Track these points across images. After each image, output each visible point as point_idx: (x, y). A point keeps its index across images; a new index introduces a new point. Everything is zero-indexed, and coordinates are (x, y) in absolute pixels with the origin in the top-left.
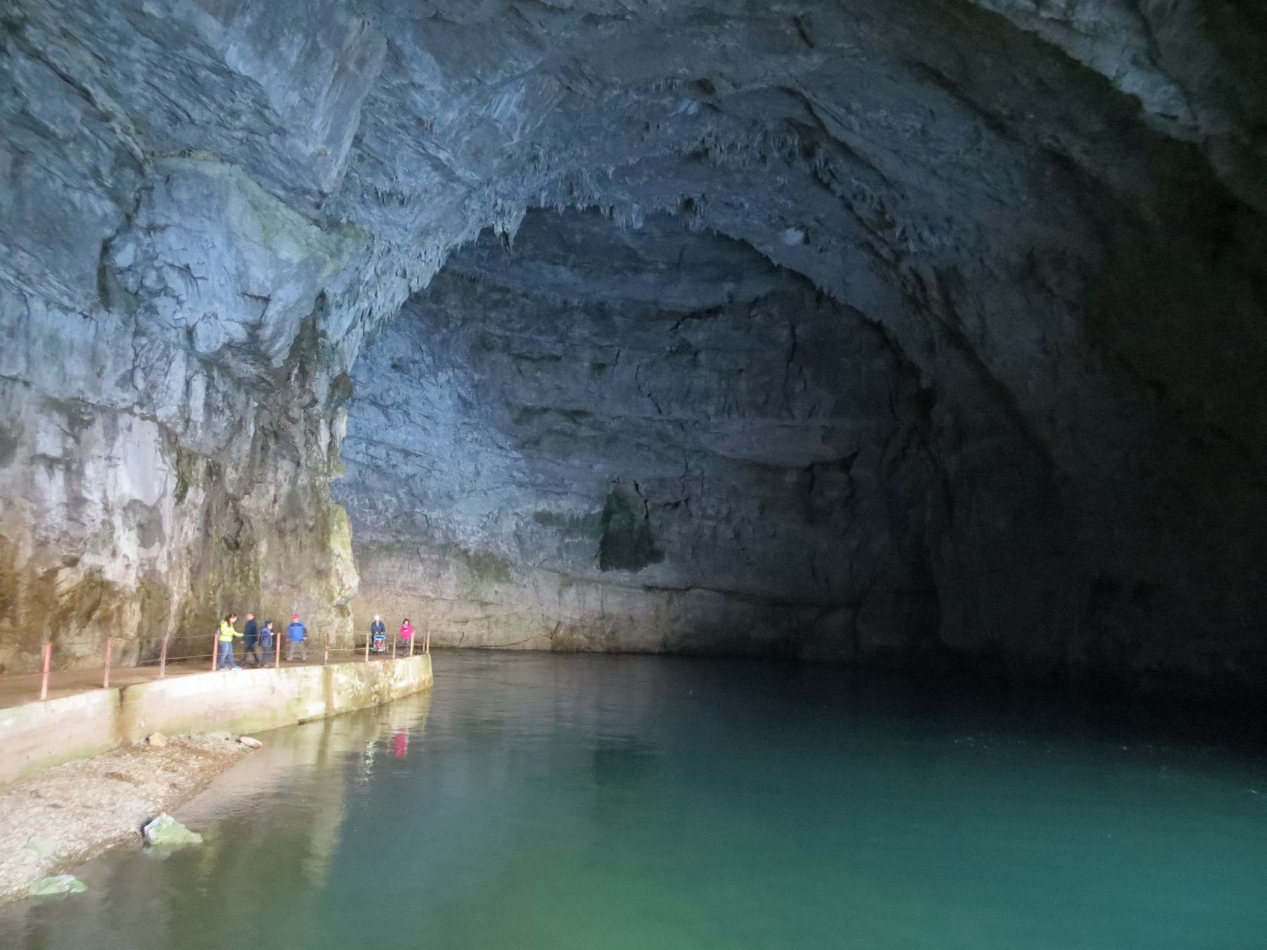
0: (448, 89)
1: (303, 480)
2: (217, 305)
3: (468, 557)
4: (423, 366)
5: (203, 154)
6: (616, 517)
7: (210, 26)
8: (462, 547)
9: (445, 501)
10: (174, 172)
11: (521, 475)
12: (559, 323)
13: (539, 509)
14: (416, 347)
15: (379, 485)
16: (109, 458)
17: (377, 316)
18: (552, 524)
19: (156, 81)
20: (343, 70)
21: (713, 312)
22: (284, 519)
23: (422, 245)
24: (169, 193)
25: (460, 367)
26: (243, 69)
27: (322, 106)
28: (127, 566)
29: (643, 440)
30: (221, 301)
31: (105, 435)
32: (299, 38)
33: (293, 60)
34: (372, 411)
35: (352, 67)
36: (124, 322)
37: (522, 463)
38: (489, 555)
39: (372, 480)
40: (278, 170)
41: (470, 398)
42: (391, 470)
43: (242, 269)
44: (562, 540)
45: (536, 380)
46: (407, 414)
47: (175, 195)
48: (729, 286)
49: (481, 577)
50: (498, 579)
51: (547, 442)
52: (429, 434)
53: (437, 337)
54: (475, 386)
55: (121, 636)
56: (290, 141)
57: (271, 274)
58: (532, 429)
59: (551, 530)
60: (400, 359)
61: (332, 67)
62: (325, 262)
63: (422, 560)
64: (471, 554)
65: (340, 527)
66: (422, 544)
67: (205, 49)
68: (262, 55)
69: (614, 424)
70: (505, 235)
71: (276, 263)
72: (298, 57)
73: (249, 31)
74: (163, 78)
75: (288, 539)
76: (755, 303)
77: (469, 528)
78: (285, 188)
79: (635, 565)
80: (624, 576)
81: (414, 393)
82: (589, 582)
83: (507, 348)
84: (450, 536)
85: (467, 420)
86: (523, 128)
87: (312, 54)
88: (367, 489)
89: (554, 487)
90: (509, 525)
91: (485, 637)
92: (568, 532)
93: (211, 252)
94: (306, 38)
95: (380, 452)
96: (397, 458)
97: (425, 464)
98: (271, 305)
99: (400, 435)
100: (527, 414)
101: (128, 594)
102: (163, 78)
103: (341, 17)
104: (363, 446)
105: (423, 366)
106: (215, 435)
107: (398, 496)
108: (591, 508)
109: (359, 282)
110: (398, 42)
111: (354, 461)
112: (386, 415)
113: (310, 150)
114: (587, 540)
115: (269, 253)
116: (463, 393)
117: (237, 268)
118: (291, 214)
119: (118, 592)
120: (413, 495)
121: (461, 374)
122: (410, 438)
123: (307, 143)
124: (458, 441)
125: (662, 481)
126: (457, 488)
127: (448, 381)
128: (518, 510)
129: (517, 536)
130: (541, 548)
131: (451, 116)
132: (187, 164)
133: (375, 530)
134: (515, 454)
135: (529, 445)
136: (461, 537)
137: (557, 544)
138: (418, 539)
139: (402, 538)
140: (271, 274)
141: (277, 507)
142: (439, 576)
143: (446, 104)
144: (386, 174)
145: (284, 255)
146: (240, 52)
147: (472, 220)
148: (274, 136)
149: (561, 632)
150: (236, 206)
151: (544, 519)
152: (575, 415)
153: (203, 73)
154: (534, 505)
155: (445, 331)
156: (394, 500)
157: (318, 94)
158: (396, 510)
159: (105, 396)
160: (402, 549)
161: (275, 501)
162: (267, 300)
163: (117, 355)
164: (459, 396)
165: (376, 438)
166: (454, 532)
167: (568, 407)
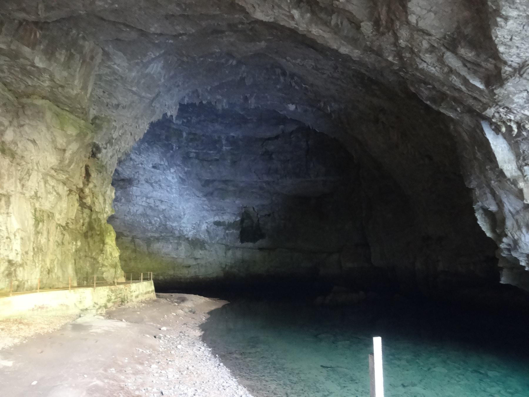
0: (130, 64)
1: (94, 216)
2: (46, 153)
3: (189, 241)
4: (164, 166)
5: (35, 96)
6: (246, 221)
7: (26, 50)
8: (186, 237)
9: (178, 219)
10: (25, 104)
11: (207, 207)
12: (217, 145)
13: (216, 220)
14: (161, 159)
15: (152, 214)
16: (8, 213)
17: (122, 151)
18: (221, 226)
19: (12, 71)
20: (84, 61)
21: (277, 137)
22: (87, 232)
23: (137, 123)
24: (24, 112)
25: (179, 166)
26: (40, 65)
27: (77, 76)
28: (17, 254)
29: (254, 190)
30: (47, 151)
31: (6, 204)
32: (64, 52)
33: (62, 60)
34: (146, 186)
35: (88, 60)
36: (11, 162)
37: (207, 202)
38: (197, 240)
39: (149, 212)
40: (64, 101)
41: (184, 178)
42: (156, 208)
43: (54, 139)
44: (225, 232)
45: (210, 169)
46: (160, 185)
47: (26, 113)
48: (281, 127)
49: (194, 248)
50: (201, 249)
51: (216, 193)
52: (169, 193)
53: (169, 155)
54: (185, 173)
55: (16, 280)
56: (66, 90)
57: (65, 140)
58: (210, 189)
59: (221, 228)
60: (155, 164)
61: (79, 61)
62: (87, 134)
63: (171, 243)
64: (190, 239)
65: (110, 234)
66: (170, 236)
67: (27, 59)
68: (49, 59)
69: (242, 185)
70: (172, 116)
71: (67, 136)
72: (65, 59)
73: (43, 50)
74: (15, 70)
75: (89, 239)
76: (292, 133)
77: (188, 229)
78: (69, 107)
79: (254, 240)
80: (250, 245)
81: (161, 178)
82: (237, 248)
83: (197, 157)
84: (181, 232)
85: (183, 187)
86: (165, 76)
87: (70, 57)
88: (147, 216)
89: (221, 211)
90: (204, 227)
91: (197, 272)
92: (227, 229)
93: (41, 133)
94: (67, 51)
95: (151, 201)
96: (158, 203)
97: (169, 205)
98: (67, 151)
99: (157, 194)
100: (207, 183)
101: (18, 264)
102: (15, 70)
103: (81, 42)
104: (145, 199)
105: (164, 166)
106: (50, 202)
107: (160, 218)
108: (236, 218)
109: (113, 138)
110: (106, 49)
111: (142, 205)
112: (152, 186)
113: (74, 92)
114: (235, 231)
115: (63, 132)
116: (181, 176)
117: (52, 138)
118: (72, 117)
119: (14, 264)
120: (165, 217)
121: (180, 168)
122: (162, 195)
123: (73, 90)
124: (181, 195)
125: (263, 205)
126: (182, 214)
127: (175, 171)
128: (207, 221)
129: (208, 231)
130: (217, 235)
131: (133, 74)
132: (29, 101)
133: (153, 232)
134: (204, 199)
135: (208, 195)
136: (185, 233)
137: (223, 233)
138: (168, 235)
139: (163, 235)
140: (65, 140)
141: (84, 227)
142: (177, 249)
143: (130, 70)
144: (115, 98)
145: (69, 132)
146: (40, 59)
147: (158, 111)
148: (60, 89)
149: (227, 269)
150: (48, 115)
151: (217, 224)
152: (225, 182)
153: (28, 67)
154: (212, 219)
155: (171, 152)
156: (158, 220)
157: (75, 71)
158: (160, 224)
159: (5, 190)
160: (162, 239)
161: (83, 225)
162: (64, 150)
163: (9, 174)
164: (180, 177)
165: (149, 196)
166: (182, 231)
167: (224, 179)
